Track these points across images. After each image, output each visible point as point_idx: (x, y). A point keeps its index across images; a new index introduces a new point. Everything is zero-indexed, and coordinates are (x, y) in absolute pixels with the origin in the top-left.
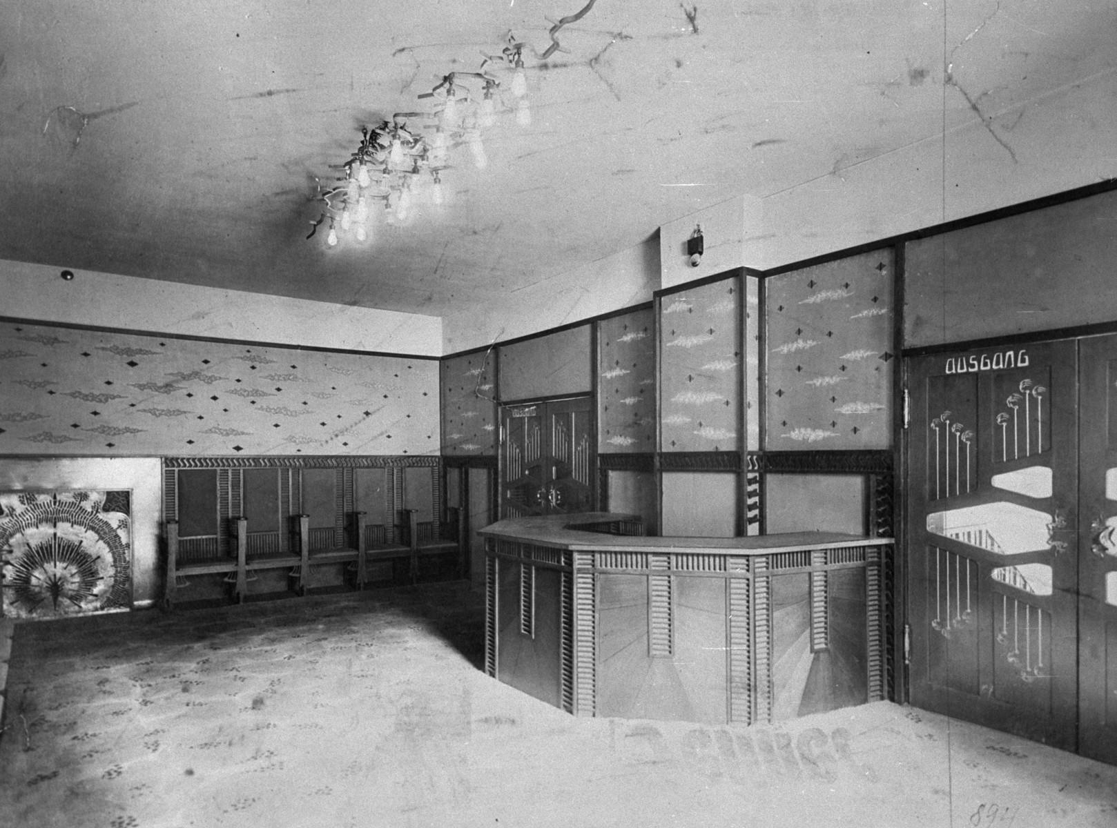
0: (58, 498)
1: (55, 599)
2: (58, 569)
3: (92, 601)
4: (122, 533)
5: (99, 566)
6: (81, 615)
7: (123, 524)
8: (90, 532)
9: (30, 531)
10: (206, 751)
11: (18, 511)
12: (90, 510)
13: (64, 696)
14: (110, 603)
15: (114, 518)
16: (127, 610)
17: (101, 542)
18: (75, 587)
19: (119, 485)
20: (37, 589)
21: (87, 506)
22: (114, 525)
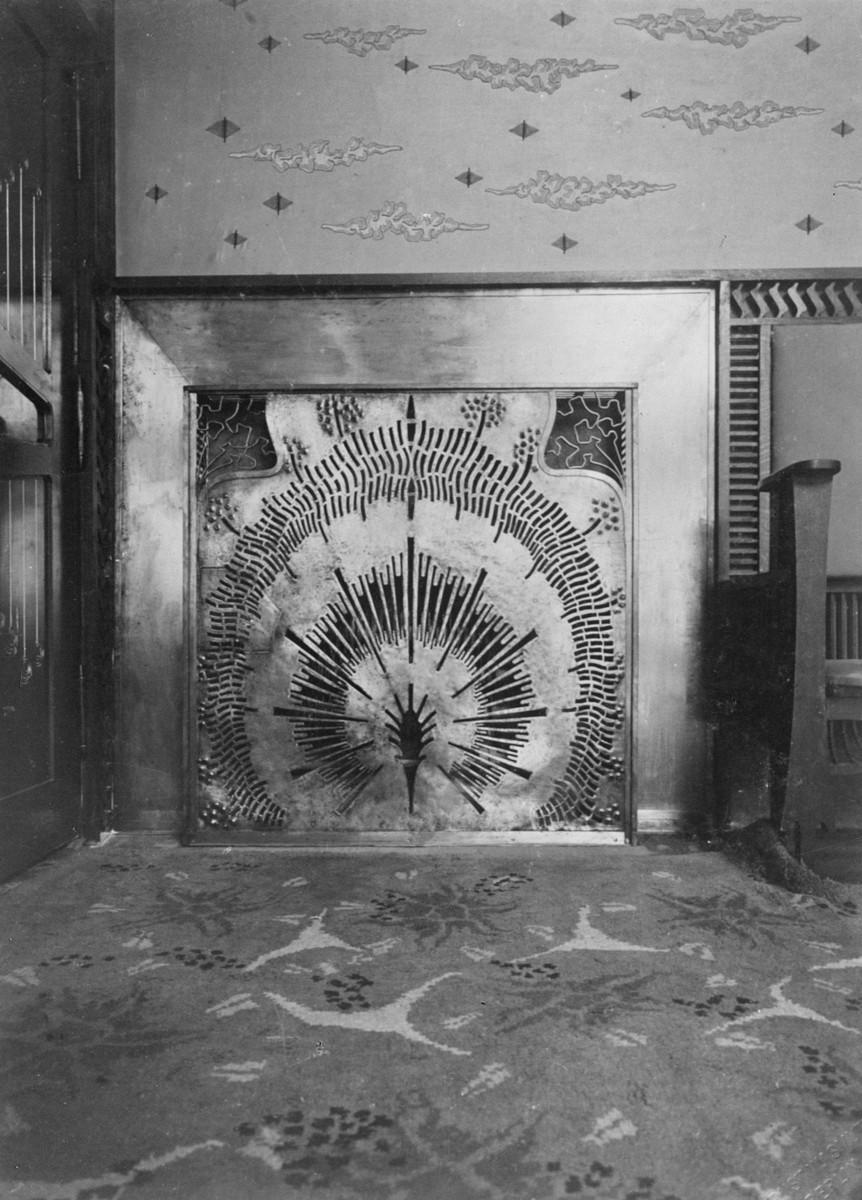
0: (420, 413)
1: (411, 773)
2: (437, 672)
3: (516, 793)
4: (600, 549)
5: (530, 664)
6: (481, 838)
7: (607, 518)
8: (510, 543)
9: (345, 526)
10: (677, 1005)
11: (313, 461)
12: (507, 460)
13: (542, 765)
14: (570, 806)
15: (577, 491)
16: (615, 838)
17: (539, 577)
18: (466, 734)
19: (596, 374)
20: (361, 733)
21: (501, 443)
22: (579, 515)
